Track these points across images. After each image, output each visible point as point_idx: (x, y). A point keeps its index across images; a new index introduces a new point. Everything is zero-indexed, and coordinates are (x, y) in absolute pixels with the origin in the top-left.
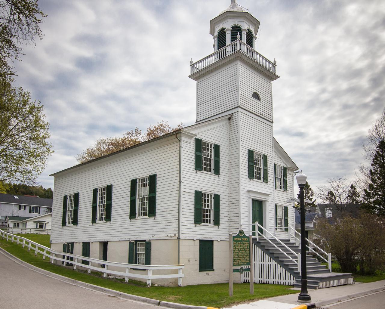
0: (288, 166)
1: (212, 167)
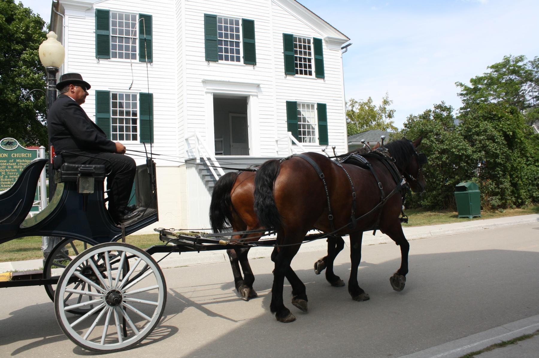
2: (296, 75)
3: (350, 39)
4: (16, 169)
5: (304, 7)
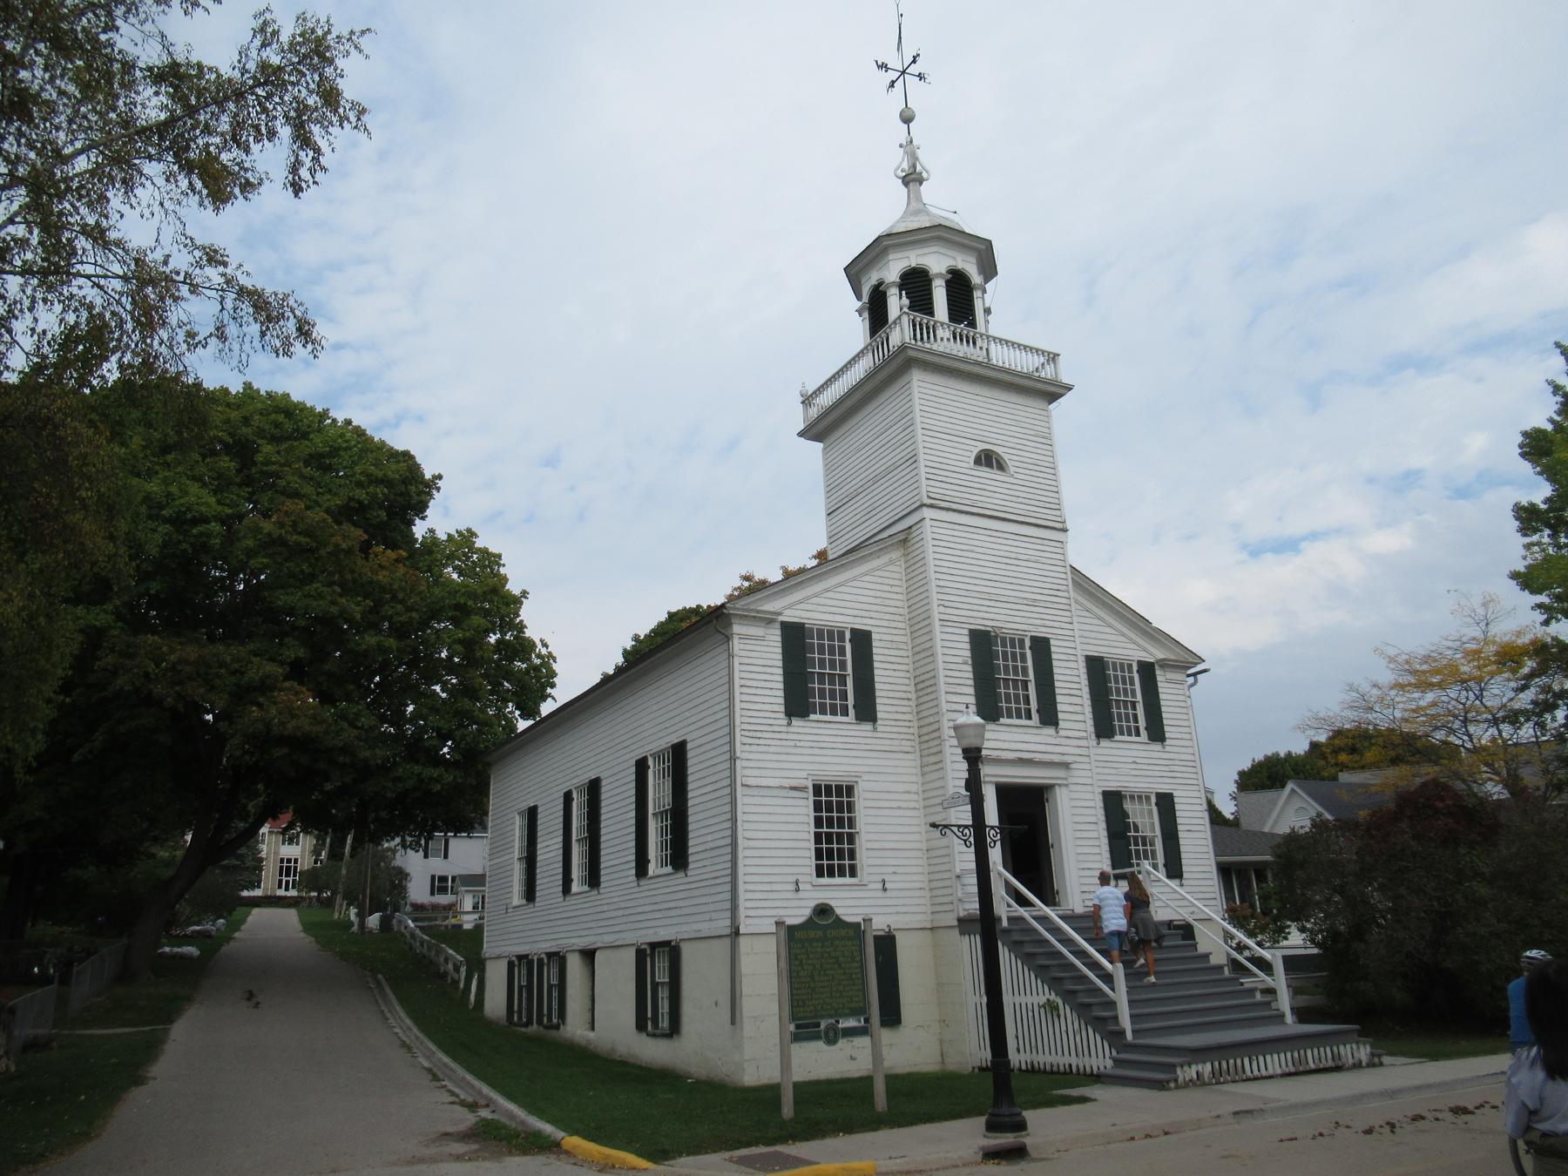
0: (1160, 655)
1: (1142, 723)
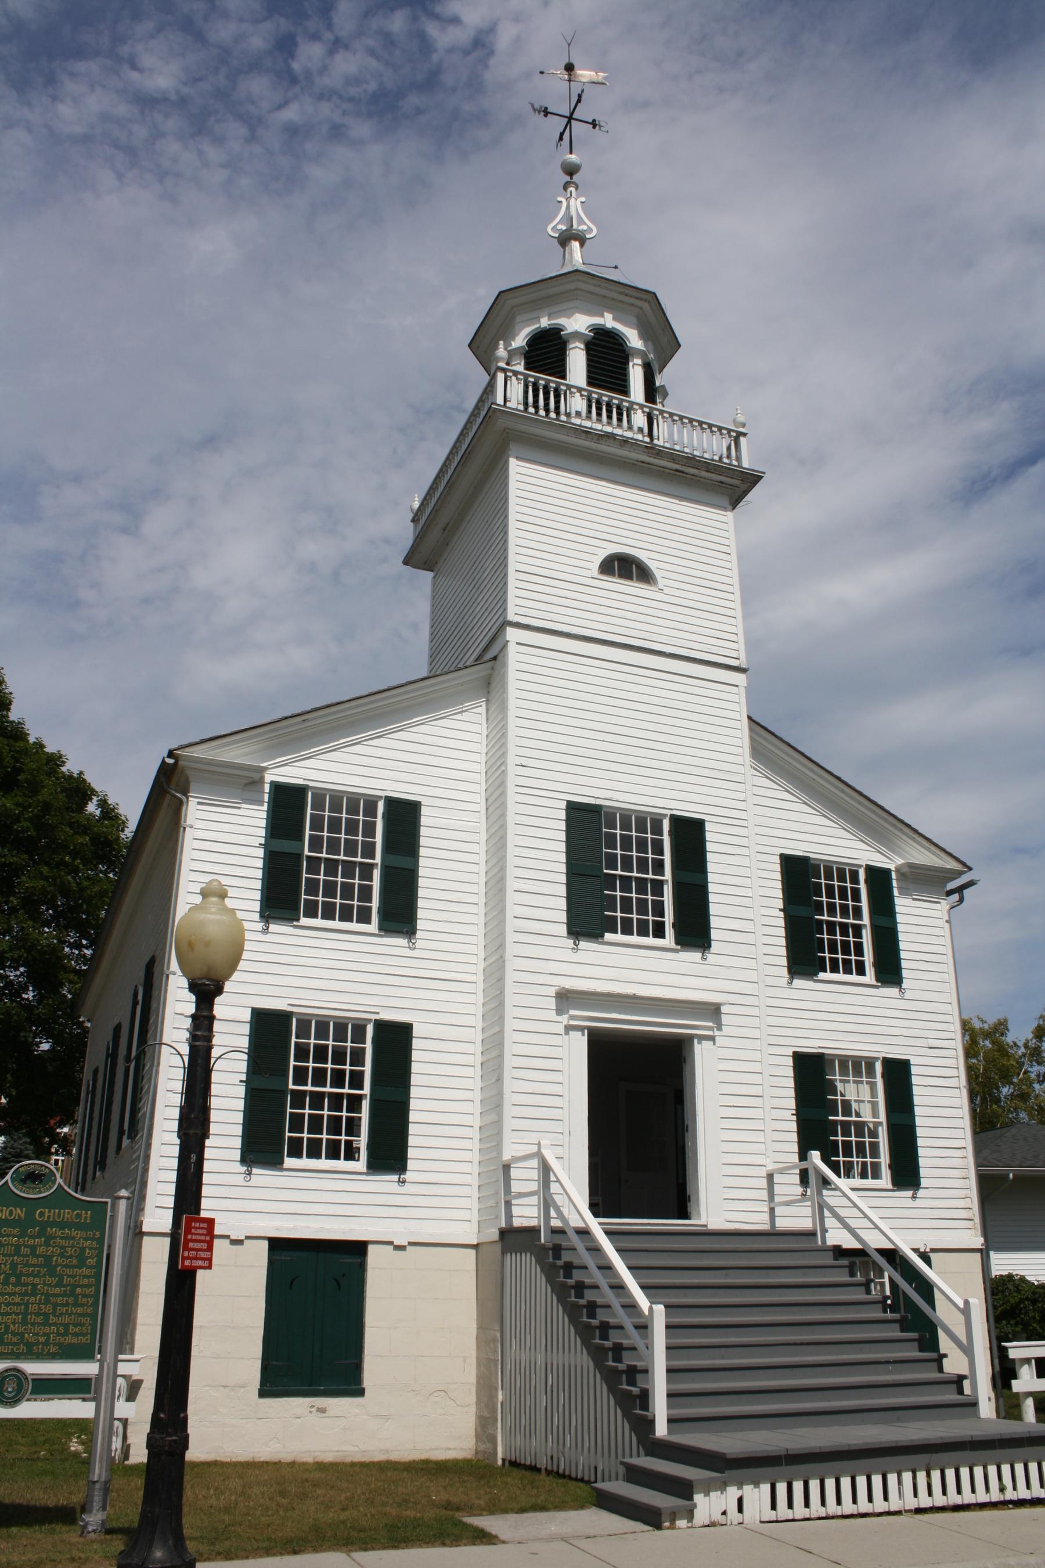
1: (868, 957)
2: (822, 975)
3: (970, 869)
4: (42, 1256)
5: (839, 779)
